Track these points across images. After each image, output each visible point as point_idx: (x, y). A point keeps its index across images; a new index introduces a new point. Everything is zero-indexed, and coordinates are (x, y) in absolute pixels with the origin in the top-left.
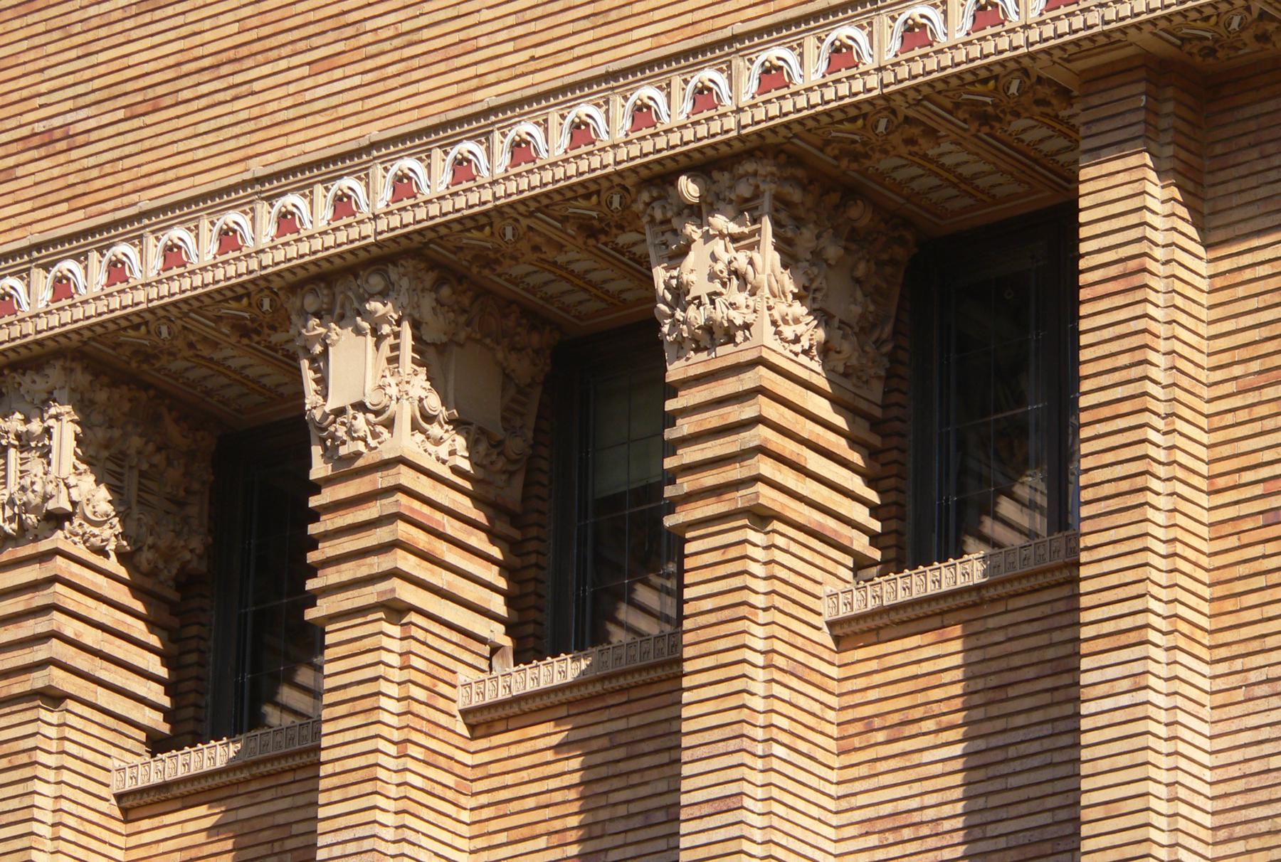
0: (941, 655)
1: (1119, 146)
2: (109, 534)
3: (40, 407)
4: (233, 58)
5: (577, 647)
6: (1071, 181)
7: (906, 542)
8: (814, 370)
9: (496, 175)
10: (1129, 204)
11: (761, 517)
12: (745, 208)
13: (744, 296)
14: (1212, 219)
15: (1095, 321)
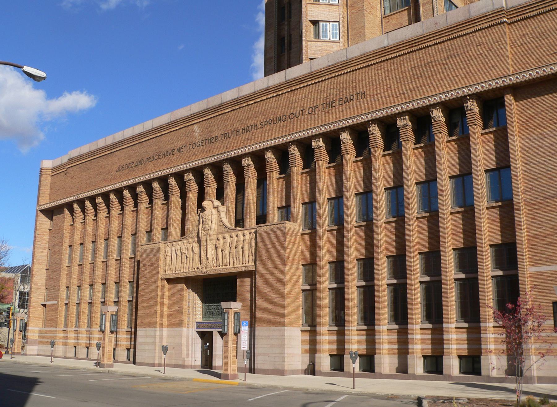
0: (491, 136)
2: (411, 127)
3: (405, 116)
4: (420, 87)
5: (390, 150)
6: (503, 98)
8: (478, 112)
9: (449, 97)
10: (509, 99)
11: (476, 125)
12: (228, 163)
13: (438, 114)
14: (516, 100)
15: (507, 109)
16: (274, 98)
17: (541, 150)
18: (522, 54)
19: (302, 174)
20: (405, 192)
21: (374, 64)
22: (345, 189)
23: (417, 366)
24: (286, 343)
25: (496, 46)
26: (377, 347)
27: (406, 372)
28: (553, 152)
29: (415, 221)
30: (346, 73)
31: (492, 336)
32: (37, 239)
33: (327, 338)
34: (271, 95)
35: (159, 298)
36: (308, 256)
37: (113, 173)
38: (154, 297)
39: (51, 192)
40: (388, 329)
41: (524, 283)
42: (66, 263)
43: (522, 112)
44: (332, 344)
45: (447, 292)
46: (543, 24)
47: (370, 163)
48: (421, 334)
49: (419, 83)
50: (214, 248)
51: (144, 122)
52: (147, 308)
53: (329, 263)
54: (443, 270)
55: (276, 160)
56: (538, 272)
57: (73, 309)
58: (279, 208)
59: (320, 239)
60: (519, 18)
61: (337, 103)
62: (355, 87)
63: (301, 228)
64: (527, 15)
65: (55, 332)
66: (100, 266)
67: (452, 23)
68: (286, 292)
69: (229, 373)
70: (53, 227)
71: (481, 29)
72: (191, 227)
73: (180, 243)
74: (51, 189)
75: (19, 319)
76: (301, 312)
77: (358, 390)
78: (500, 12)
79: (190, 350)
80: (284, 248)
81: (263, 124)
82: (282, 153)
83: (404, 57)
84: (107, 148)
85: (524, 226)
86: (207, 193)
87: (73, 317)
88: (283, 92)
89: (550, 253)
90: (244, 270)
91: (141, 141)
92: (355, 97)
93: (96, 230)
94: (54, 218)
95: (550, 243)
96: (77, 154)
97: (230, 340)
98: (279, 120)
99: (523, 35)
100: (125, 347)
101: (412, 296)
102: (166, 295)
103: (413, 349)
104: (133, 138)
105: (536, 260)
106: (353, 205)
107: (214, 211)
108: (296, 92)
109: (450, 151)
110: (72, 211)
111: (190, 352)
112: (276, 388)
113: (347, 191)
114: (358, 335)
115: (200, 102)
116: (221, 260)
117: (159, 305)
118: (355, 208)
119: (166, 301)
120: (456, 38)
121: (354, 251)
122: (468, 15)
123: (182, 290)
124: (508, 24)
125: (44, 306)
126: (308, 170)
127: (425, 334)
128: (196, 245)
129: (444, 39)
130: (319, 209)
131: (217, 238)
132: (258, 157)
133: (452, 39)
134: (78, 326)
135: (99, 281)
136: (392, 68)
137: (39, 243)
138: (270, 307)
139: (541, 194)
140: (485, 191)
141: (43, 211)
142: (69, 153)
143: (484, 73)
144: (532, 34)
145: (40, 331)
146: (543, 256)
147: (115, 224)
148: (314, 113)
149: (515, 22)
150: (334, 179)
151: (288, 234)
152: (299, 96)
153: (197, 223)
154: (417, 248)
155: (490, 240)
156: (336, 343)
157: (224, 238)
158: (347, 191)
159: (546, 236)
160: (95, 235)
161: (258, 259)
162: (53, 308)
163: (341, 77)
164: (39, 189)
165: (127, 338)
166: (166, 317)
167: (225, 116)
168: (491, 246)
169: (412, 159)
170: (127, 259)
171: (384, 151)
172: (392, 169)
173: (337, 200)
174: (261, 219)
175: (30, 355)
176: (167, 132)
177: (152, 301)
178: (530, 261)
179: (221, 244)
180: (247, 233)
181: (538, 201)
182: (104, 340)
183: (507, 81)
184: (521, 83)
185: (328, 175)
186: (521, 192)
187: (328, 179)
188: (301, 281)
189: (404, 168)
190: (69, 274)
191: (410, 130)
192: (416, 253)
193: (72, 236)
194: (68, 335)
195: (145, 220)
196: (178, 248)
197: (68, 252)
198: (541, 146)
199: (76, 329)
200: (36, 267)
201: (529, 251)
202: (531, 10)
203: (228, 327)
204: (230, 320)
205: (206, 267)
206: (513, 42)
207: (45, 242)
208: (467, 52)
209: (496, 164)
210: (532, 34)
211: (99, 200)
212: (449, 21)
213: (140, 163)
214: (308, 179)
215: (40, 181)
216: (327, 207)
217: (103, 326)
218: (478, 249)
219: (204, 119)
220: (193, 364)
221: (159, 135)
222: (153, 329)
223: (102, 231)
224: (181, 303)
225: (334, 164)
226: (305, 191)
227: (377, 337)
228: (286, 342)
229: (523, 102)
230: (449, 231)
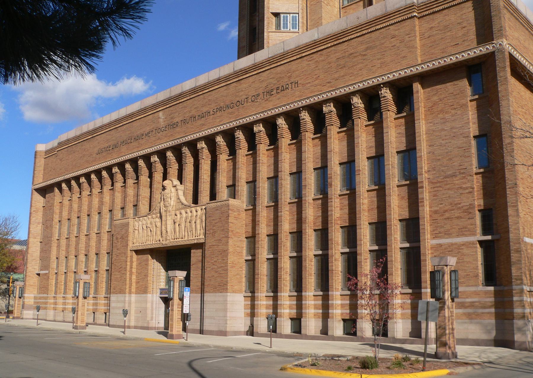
0: (403, 121)
1: (416, 82)
2: (335, 112)
5: (373, 120)
7: (369, 120)
8: (392, 99)
9: (366, 85)
10: (417, 87)
11: (389, 111)
13: (386, 94)
14: (423, 88)
15: (415, 95)
16: (225, 88)
17: (443, 133)
18: (429, 45)
19: (246, 155)
20: (329, 172)
21: (306, 56)
22: (280, 170)
23: (337, 328)
24: (228, 307)
25: (407, 38)
26: (303, 311)
27: (355, 334)
28: (452, 135)
29: (337, 198)
30: (283, 64)
31: (399, 301)
32: (33, 215)
33: (265, 303)
34: (222, 85)
35: (128, 267)
36: (250, 230)
37: (94, 155)
38: (124, 267)
39: (44, 173)
40: (314, 296)
41: (425, 254)
42: (56, 236)
43: (428, 99)
44: (269, 309)
45: (361, 262)
46: (447, 18)
47: (301, 146)
48: (341, 300)
49: (342, 72)
50: (173, 223)
51: (209, 71)
52: (119, 276)
53: (268, 235)
54: (358, 242)
55: (225, 143)
56: (437, 245)
57: (62, 278)
58: (228, 187)
59: (259, 214)
60: (427, 13)
61: (275, 91)
62: (290, 77)
63: (245, 205)
64: (434, 9)
65: (46, 298)
66: (83, 238)
67: (371, 17)
68: (229, 262)
69: (174, 333)
70: (46, 204)
71: (395, 23)
72: (158, 204)
73: (145, 218)
74: (44, 170)
75: (18, 287)
76: (244, 280)
77: (274, 348)
78: (410, 7)
79: (154, 313)
80: (228, 223)
81: (215, 111)
82: (270, 124)
83: (331, 49)
84: (89, 133)
85: (427, 203)
86: (169, 173)
87: (62, 285)
88: (231, 82)
89: (448, 227)
90: (196, 242)
91: (117, 126)
92: (290, 86)
93: (80, 207)
94: (47, 196)
95: (448, 218)
96: (65, 139)
97: (175, 304)
98: (228, 107)
99: (431, 28)
100: (103, 311)
101: (333, 266)
102: (135, 264)
103: (333, 313)
104: (110, 124)
105: (436, 234)
106: (287, 184)
107: (173, 190)
108: (242, 81)
109: (368, 134)
110: (61, 190)
111: (154, 316)
112: (208, 346)
113: (282, 171)
114: (290, 300)
115: (165, 91)
116: (178, 234)
117: (128, 273)
118: (289, 186)
119: (134, 270)
120: (374, 31)
121: (287, 226)
122: (384, 10)
123: (147, 260)
124: (419, 18)
125: (39, 274)
126: (319, 135)
127: (344, 300)
128: (158, 220)
129: (364, 32)
130: (259, 188)
131: (174, 214)
132: (210, 140)
133: (371, 32)
134: (65, 293)
135: (83, 252)
136: (321, 59)
137: (34, 219)
138: (216, 275)
139: (442, 173)
140: (396, 170)
141: (37, 190)
142: (59, 137)
143: (396, 63)
144: (438, 27)
145: (35, 298)
146: (442, 230)
147: (96, 201)
148: (256, 101)
149: (424, 16)
150: (272, 161)
151: (232, 210)
152: (244, 85)
153: (160, 200)
154: (339, 222)
155: (400, 215)
156: (321, 307)
157: (181, 214)
158: (282, 171)
159: (445, 211)
160: (79, 211)
161: (207, 232)
162: (45, 277)
163: (278, 68)
164: (34, 170)
165: (105, 304)
166: (134, 285)
167: (185, 104)
168: (400, 220)
169: (337, 142)
170: (105, 233)
171: (314, 134)
172: (320, 151)
173: (348, 165)
174: (213, 196)
175: (26, 319)
176: (137, 118)
177: (122, 270)
178: (432, 234)
179: (178, 219)
180: (199, 208)
181: (439, 180)
182: (78, 305)
183: (414, 71)
184: (427, 72)
185: (268, 156)
186: (425, 172)
187: (268, 160)
188: (245, 252)
189: (328, 150)
190: (59, 246)
191: (335, 115)
192: (338, 227)
193: (61, 213)
194: (57, 301)
195: (120, 197)
196: (144, 222)
197: (58, 227)
198: (443, 130)
199: (64, 296)
200: (31, 240)
201: (430, 225)
202: (438, 5)
203: (173, 293)
204: (175, 287)
205: (166, 240)
206: (422, 34)
207: (40, 218)
208: (383, 44)
209: (406, 146)
210: (438, 27)
211: (115, 170)
212: (369, 15)
213: (116, 146)
214: (252, 160)
215: (35, 163)
216: (266, 185)
217: (77, 292)
218: (388, 223)
219: (168, 106)
220: (157, 326)
221: (131, 121)
222: (124, 295)
223: (85, 208)
224: (146, 272)
225: (345, 129)
226: (249, 171)
227: (303, 302)
228: (229, 306)
229: (429, 89)
230: (365, 207)
